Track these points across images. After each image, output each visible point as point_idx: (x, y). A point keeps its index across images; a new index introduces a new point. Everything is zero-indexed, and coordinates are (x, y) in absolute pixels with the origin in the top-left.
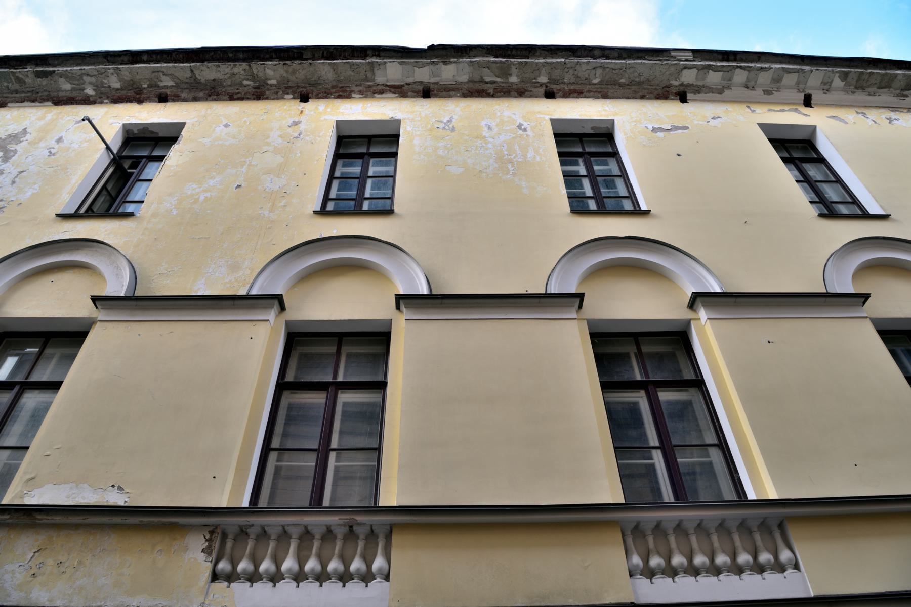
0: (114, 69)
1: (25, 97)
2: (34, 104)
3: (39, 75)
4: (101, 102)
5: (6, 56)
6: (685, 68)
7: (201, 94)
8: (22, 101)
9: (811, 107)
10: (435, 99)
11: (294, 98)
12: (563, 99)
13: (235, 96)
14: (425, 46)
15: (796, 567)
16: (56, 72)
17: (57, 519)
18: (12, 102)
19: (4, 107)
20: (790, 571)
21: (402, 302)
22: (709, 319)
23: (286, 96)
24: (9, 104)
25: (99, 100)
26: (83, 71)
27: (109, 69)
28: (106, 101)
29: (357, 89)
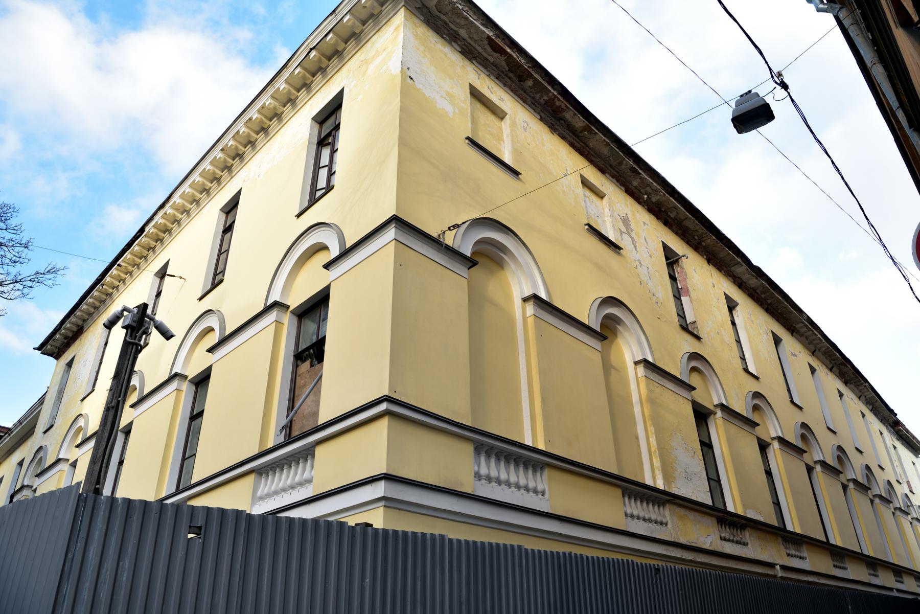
0: (664, 194)
1: (616, 176)
2: (611, 178)
3: (633, 170)
4: (643, 206)
5: (673, 187)
6: (802, 323)
7: (679, 232)
8: (613, 177)
9: (846, 386)
10: (669, 230)
11: (706, 259)
12: (694, 251)
13: (689, 243)
14: (755, 263)
15: (543, 494)
16: (641, 175)
17: (763, 528)
18: (608, 173)
19: (602, 173)
20: (483, 481)
21: (391, 233)
22: (645, 376)
23: (704, 256)
24: (607, 174)
25: (643, 204)
26: (651, 185)
27: (662, 192)
28: (646, 207)
29: (725, 269)
